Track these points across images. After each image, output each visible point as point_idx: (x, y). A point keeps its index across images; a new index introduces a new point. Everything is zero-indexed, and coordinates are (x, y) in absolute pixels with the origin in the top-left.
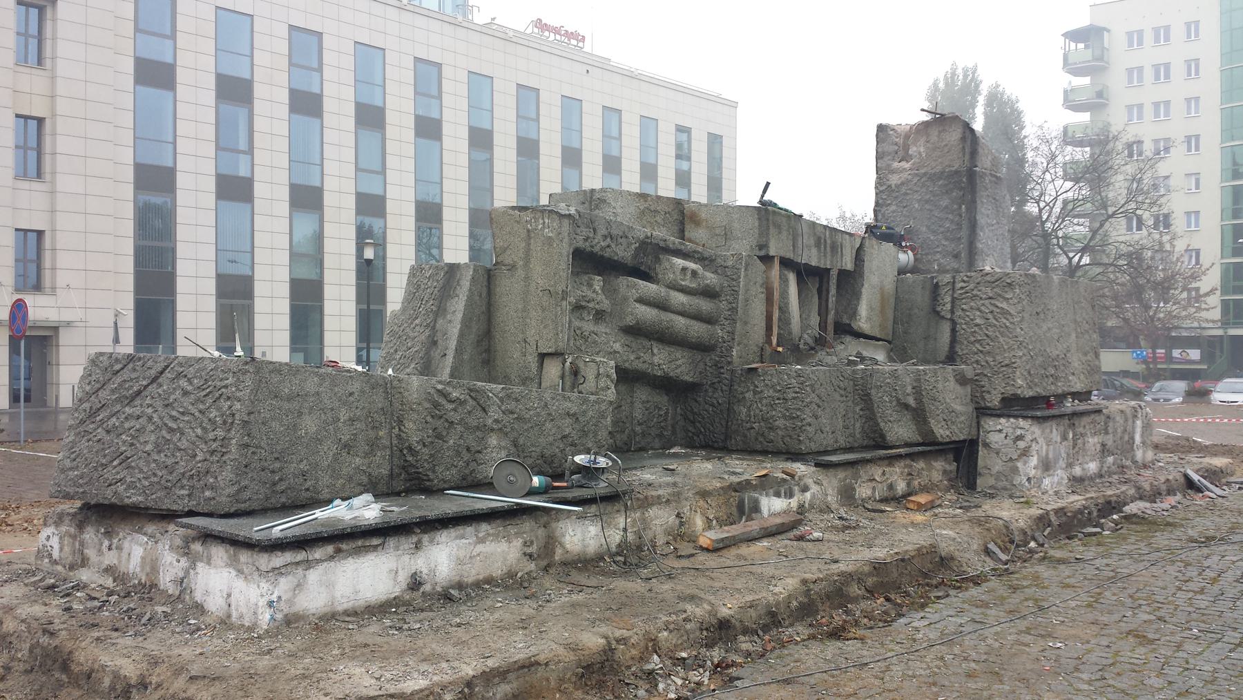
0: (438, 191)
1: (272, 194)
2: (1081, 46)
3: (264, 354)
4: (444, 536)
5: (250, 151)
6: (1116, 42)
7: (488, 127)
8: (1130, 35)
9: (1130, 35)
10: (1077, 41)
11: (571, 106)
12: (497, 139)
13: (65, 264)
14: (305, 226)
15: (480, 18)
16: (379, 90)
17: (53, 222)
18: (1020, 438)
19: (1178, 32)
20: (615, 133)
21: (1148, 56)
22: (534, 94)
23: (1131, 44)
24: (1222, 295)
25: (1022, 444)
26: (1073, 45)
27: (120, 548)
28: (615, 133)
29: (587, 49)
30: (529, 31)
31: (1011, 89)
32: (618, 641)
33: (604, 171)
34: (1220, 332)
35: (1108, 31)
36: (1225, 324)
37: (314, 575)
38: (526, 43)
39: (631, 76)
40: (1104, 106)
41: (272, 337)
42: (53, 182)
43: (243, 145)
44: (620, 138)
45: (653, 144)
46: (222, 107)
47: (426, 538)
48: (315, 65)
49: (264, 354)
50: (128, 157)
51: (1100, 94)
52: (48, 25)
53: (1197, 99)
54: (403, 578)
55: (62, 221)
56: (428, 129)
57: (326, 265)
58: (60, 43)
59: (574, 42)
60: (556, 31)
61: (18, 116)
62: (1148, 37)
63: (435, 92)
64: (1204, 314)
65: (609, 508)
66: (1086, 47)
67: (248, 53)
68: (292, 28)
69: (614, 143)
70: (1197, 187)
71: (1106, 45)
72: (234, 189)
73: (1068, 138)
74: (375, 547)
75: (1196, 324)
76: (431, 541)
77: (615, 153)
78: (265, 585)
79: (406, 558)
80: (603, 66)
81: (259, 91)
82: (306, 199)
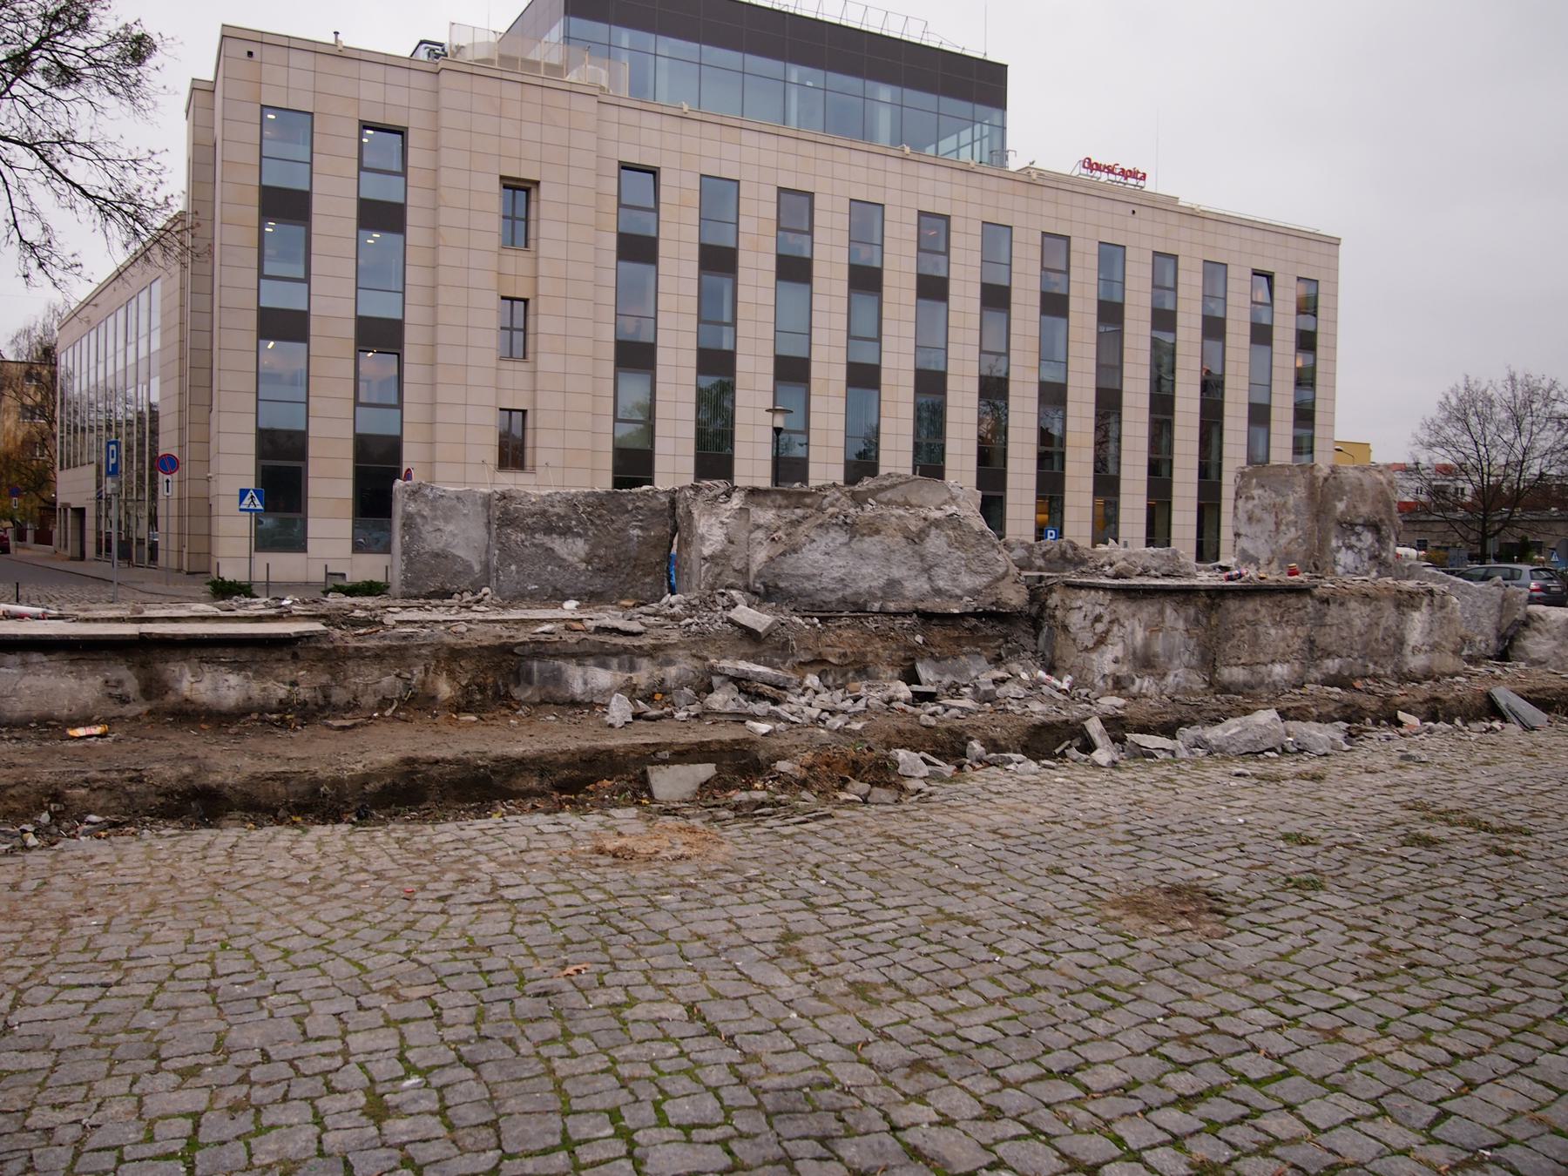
1: (828, 372)
11: (1111, 256)
13: (544, 445)
14: (634, 390)
15: (1014, 164)
16: (1117, 286)
17: (534, 401)
18: (1098, 619)
20: (1169, 283)
22: (1064, 242)
25: (1100, 627)
28: (1169, 283)
29: (1149, 186)
33: (1252, 341)
42: (535, 362)
43: (727, 318)
44: (1175, 289)
45: (1118, 277)
52: (533, 205)
55: (544, 401)
56: (1054, 305)
57: (657, 432)
58: (543, 224)
59: (1131, 181)
60: (1110, 170)
61: (503, 298)
72: (792, 372)
80: (1166, 206)
81: (744, 259)
82: (863, 377)
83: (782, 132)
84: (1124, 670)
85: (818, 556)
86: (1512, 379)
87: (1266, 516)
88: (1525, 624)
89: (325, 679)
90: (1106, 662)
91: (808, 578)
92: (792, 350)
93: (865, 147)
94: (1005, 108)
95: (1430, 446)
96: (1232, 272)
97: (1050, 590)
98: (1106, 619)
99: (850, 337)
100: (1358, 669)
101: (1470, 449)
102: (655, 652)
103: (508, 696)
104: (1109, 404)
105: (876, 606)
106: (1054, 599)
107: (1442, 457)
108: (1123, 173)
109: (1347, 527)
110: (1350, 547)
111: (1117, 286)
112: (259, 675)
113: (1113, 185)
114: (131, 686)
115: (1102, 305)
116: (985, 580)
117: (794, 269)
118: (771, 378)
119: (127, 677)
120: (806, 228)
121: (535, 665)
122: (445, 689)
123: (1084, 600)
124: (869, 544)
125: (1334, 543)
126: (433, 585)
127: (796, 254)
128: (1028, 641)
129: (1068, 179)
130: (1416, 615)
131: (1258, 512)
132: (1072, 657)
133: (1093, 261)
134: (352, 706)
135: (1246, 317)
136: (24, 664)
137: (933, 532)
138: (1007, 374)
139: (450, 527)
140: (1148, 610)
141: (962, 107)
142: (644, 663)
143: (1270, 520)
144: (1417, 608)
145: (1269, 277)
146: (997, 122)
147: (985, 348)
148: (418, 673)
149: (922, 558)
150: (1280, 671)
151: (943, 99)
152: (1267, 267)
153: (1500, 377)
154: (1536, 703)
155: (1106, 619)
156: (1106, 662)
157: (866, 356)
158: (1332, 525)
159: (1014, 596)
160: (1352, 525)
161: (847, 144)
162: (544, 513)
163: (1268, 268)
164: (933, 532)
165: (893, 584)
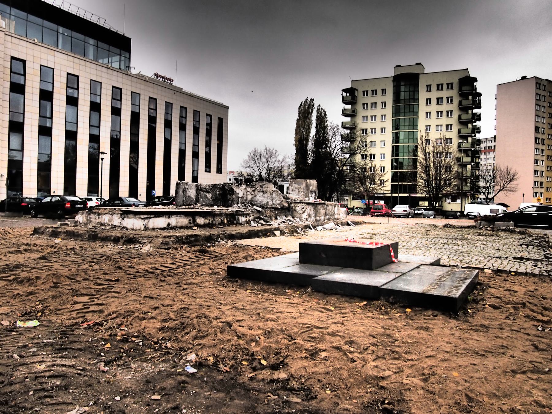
2: (348, 94)
3: (54, 192)
5: (51, 118)
6: (360, 95)
15: (134, 71)
16: (98, 97)
18: (303, 208)
20: (184, 116)
23: (364, 95)
24: (391, 182)
25: (303, 210)
26: (345, 94)
29: (174, 84)
30: (153, 77)
33: (180, 129)
34: (390, 195)
35: (357, 90)
36: (392, 192)
37: (151, 220)
41: (57, 186)
43: (48, 115)
48: (76, 87)
49: (54, 192)
50: (7, 118)
53: (385, 115)
59: (169, 82)
60: (163, 77)
64: (384, 188)
68: (68, 74)
69: (184, 119)
70: (384, 145)
73: (344, 126)
75: (382, 192)
83: (56, 50)
84: (307, 217)
86: (266, 149)
90: (305, 216)
93: (96, 63)
97: (291, 203)
102: (249, 214)
104: (115, 143)
107: (248, 170)
108: (167, 79)
109: (311, 192)
114: (192, 221)
117: (72, 101)
120: (119, 98)
122: (226, 221)
124: (265, 195)
126: (188, 203)
129: (150, 78)
132: (298, 215)
141: (118, 51)
143: (297, 191)
145: (211, 116)
146: (127, 56)
147: (91, 124)
156: (305, 216)
157: (95, 132)
161: (79, 57)
163: (211, 114)
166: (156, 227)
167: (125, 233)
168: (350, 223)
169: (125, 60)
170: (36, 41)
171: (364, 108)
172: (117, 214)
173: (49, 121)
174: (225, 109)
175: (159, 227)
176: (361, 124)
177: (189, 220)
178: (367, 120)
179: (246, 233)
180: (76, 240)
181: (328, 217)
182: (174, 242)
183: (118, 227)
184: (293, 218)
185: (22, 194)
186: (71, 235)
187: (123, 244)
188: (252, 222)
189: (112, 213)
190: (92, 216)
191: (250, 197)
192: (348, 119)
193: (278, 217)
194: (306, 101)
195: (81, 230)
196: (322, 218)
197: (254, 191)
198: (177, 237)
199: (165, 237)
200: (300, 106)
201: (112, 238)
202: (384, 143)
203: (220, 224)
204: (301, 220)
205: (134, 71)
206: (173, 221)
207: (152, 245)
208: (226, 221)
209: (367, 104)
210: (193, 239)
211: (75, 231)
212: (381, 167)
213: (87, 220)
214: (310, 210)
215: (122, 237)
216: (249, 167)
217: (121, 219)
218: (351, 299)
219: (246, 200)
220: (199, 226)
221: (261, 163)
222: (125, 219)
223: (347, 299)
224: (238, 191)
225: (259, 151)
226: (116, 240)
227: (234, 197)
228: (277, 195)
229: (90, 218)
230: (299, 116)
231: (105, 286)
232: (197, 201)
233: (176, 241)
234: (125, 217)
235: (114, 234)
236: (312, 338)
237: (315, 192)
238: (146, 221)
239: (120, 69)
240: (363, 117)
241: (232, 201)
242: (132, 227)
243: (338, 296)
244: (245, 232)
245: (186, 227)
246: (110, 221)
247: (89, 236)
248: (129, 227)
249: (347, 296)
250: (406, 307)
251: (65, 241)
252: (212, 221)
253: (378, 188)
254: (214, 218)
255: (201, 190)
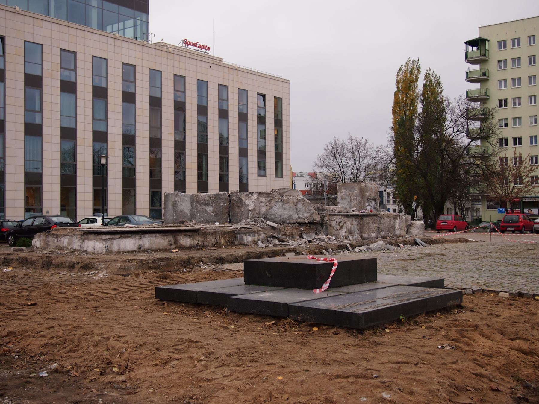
0: (133, 129)
2: (475, 48)
3: (47, 212)
4: (147, 236)
5: (41, 111)
6: (492, 47)
7: (159, 96)
8: (499, 42)
9: (499, 42)
10: (472, 46)
12: (164, 102)
15: (154, 39)
16: (104, 80)
18: (340, 222)
19: (524, 41)
20: (225, 98)
21: (509, 53)
23: (500, 48)
25: (341, 224)
26: (470, 48)
27: (60, 241)
29: (211, 53)
31: (437, 71)
32: (191, 258)
33: (219, 117)
35: (488, 41)
37: (115, 242)
38: (178, 53)
39: (233, 68)
40: (486, 80)
43: (37, 108)
44: (227, 100)
46: (29, 90)
47: (142, 236)
48: (73, 68)
49: (47, 212)
51: (484, 74)
53: (535, 76)
54: (137, 245)
56: (129, 98)
59: (204, 50)
60: (195, 45)
62: (509, 44)
63: (132, 80)
65: (194, 234)
66: (478, 49)
67: (40, 63)
68: (61, 50)
69: (225, 103)
70: (535, 123)
71: (487, 48)
74: (129, 237)
75: (533, 195)
76: (144, 237)
77: (225, 108)
78: (104, 243)
79: (137, 240)
80: (218, 62)
81: (45, 81)
84: (347, 234)
85: (276, 209)
86: (351, 139)
87: (347, 197)
88: (410, 226)
89: (203, 239)
90: (343, 232)
91: (273, 215)
92: (68, 124)
94: (148, 14)
95: (322, 167)
96: (249, 93)
97: (325, 216)
98: (343, 222)
99: (94, 119)
100: (387, 235)
101: (337, 168)
102: (257, 232)
103: (234, 243)
105: (288, 222)
106: (326, 219)
109: (369, 200)
110: (369, 205)
111: (204, 99)
112: (193, 239)
113: (195, 51)
114: (173, 242)
115: (199, 106)
116: (309, 214)
117: (68, 87)
118: (59, 137)
119: (171, 238)
121: (238, 236)
122: (223, 242)
123: (336, 219)
124: (287, 206)
125: (366, 204)
126: (180, 220)
127: (68, 80)
128: (321, 229)
129: (174, 47)
130: (397, 221)
131: (345, 196)
132: (334, 232)
133: (195, 88)
134: (208, 246)
135: (256, 113)
136: (156, 237)
137: (299, 203)
138: (135, 133)
139: (184, 204)
140: (350, 220)
141: (130, 12)
142: (256, 235)
143: (348, 199)
144: (397, 219)
145: (264, 96)
146: (144, 19)
148: (218, 238)
149: (297, 209)
150: (373, 235)
151: (121, 7)
152: (263, 92)
153: (346, 138)
154: (424, 241)
155: (343, 222)
156: (343, 232)
157: (101, 128)
158: (366, 199)
159: (318, 218)
160: (370, 199)
162: (204, 199)
164: (299, 203)
165: (290, 216)
166: (122, 250)
167: (81, 258)
168: (418, 240)
169: (141, 25)
170: (18, 9)
171: (500, 67)
172: (77, 235)
173: (38, 116)
174: (284, 84)
175: (126, 250)
176: (496, 93)
177: (169, 241)
178: (506, 86)
179: (243, 256)
180: (28, 268)
181: (383, 233)
182: (135, 267)
183: (78, 251)
184: (327, 235)
185: (4, 216)
186: (24, 262)
187: (79, 271)
188: (260, 242)
189: (71, 235)
190: (50, 239)
191: (264, 209)
192: (477, 86)
193: (304, 236)
194: (407, 65)
195: (35, 256)
196: (373, 235)
197: (270, 201)
198: (141, 261)
199: (125, 261)
200: (399, 72)
201: (67, 264)
202: (535, 120)
203: (213, 245)
204: (337, 238)
205: (154, 39)
206: (146, 242)
207: (108, 270)
208: (223, 242)
209: (505, 61)
210: (162, 263)
211: (28, 258)
212: (532, 157)
213: (45, 244)
214: (352, 224)
215: (78, 263)
216: (327, 166)
217: (81, 241)
218: (263, 318)
219: (259, 214)
220: (182, 248)
221: (344, 159)
222: (86, 241)
223: (259, 319)
224: (247, 202)
225: (341, 142)
226: (71, 267)
227: (243, 210)
228: (304, 205)
229: (48, 241)
230: (398, 88)
231: (16, 310)
232: (192, 216)
233: (140, 266)
234: (85, 239)
235: (68, 260)
236: (177, 350)
237: (375, 200)
238: (109, 243)
239: (135, 38)
240: (500, 81)
241: (241, 216)
242: (93, 251)
243: (251, 316)
244: (240, 254)
245: (165, 250)
246: (69, 243)
247: (42, 263)
248: (90, 250)
249: (260, 315)
250: (313, 326)
251: (17, 270)
252: (203, 242)
253: (526, 189)
254: (205, 237)
255: (198, 202)
